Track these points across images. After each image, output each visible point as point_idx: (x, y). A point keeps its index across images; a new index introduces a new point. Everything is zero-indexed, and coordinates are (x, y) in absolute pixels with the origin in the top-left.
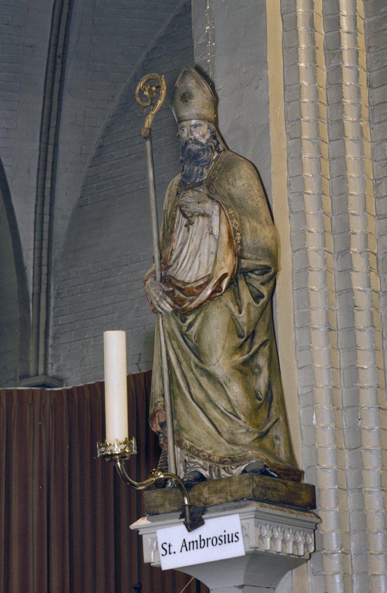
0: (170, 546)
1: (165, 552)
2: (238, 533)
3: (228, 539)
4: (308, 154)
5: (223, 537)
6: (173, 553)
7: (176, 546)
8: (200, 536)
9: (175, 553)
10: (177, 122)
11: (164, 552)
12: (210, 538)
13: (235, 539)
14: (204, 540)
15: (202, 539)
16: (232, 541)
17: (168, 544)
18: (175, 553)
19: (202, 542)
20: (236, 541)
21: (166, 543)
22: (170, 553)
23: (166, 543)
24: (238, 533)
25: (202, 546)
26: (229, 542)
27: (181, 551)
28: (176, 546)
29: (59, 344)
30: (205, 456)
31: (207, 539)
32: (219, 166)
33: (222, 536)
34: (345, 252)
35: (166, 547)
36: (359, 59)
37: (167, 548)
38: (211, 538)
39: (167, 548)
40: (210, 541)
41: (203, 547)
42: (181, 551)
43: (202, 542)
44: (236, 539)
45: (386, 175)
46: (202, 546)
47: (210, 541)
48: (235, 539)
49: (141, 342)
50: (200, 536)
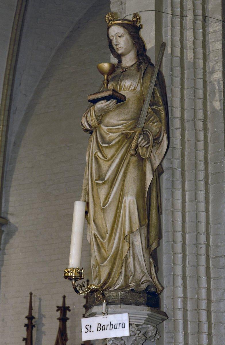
0: (90, 327)
1: (87, 330)
4: (125, 124)
6: (92, 331)
7: (94, 328)
8: (110, 322)
9: (93, 331)
12: (121, 323)
14: (112, 325)
15: (111, 324)
17: (89, 326)
18: (93, 331)
19: (111, 326)
21: (88, 325)
22: (90, 332)
23: (88, 325)
31: (107, 325)
32: (103, 192)
36: (195, 175)
38: (122, 324)
40: (121, 325)
41: (112, 329)
45: (224, 160)
46: (116, 325)
47: (121, 325)
49: (176, 287)
50: (110, 322)
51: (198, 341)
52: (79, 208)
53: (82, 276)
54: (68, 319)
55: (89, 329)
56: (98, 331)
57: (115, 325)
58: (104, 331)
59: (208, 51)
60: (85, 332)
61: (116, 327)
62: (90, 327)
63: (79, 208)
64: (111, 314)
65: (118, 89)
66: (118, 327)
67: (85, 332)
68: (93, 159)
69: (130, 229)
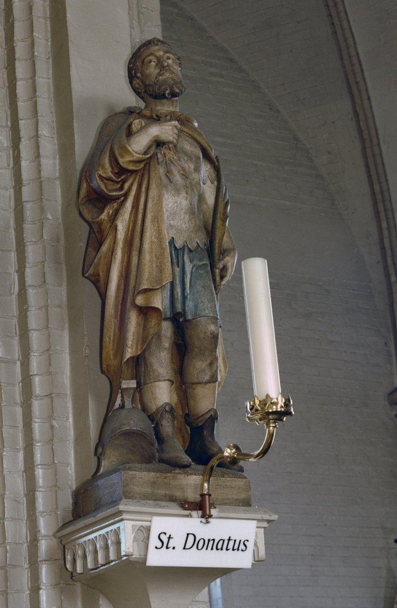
0: (169, 538)
2: (248, 541)
3: (240, 546)
5: (240, 549)
6: (172, 548)
7: (178, 542)
9: (174, 548)
11: (159, 544)
13: (242, 547)
16: (238, 550)
17: (168, 536)
18: (174, 548)
20: (242, 550)
21: (165, 534)
22: (167, 548)
23: (165, 534)
24: (248, 541)
26: (227, 549)
28: (178, 542)
33: (242, 550)
35: (164, 538)
44: (244, 548)
48: (242, 547)
51: (210, 606)
54: (213, 419)
55: (165, 543)
56: (184, 548)
57: (202, 548)
58: (220, 550)
59: (95, 514)
60: (156, 548)
61: (219, 547)
62: (169, 538)
65: (143, 122)
66: (225, 547)
67: (156, 548)
68: (125, 240)
69: (186, 361)
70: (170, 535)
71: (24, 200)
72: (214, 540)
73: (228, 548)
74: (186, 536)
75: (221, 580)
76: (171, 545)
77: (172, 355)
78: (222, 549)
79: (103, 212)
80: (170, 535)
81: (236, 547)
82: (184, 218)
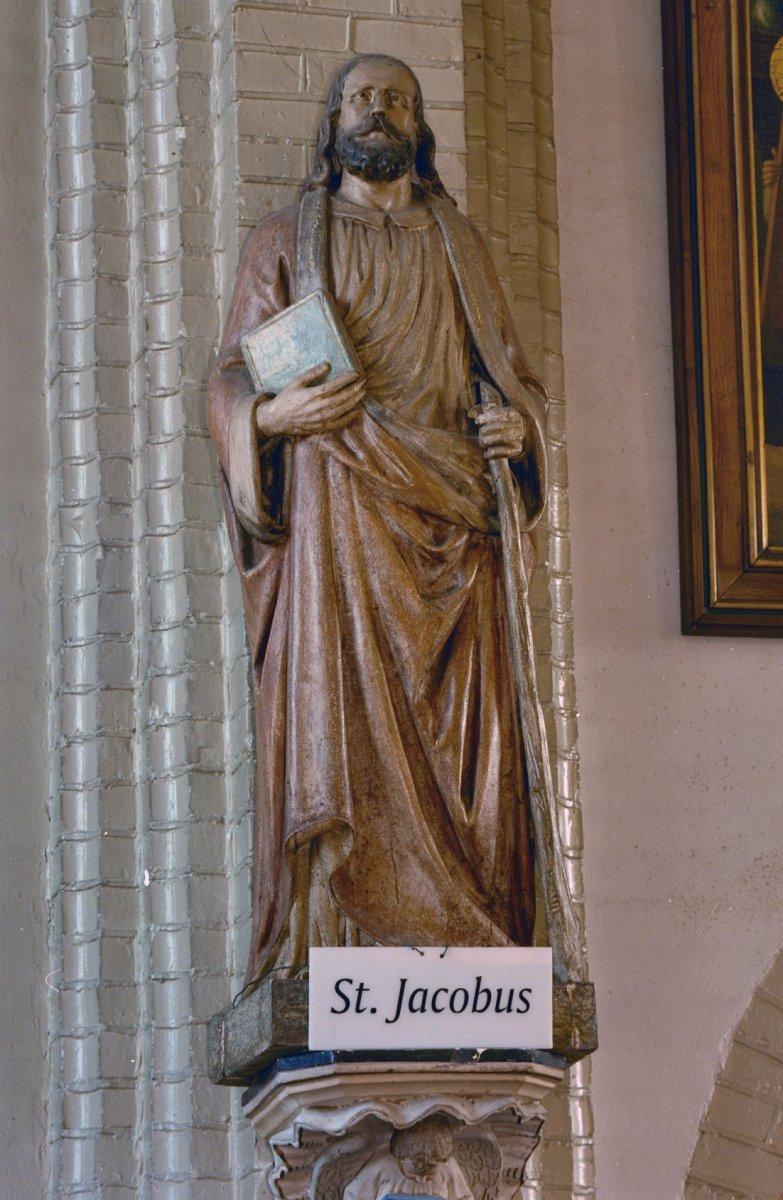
0: (361, 989)
2: (530, 991)
5: (514, 1007)
6: (368, 1011)
7: (382, 997)
8: (479, 979)
10: (529, 529)
13: (517, 1003)
14: (488, 991)
15: (482, 988)
16: (509, 1010)
17: (356, 985)
18: (374, 1011)
19: (483, 998)
20: (519, 1011)
21: (350, 981)
22: (358, 1010)
23: (350, 981)
24: (530, 991)
25: (481, 1004)
27: (403, 982)
29: (269, 181)
30: (507, 1154)
33: (519, 1011)
34: (560, 840)
35: (350, 991)
37: (353, 996)
39: (353, 996)
42: (403, 982)
43: (483, 998)
44: (523, 1007)
46: (480, 1006)
48: (517, 1003)
50: (479, 979)
52: (761, 534)
53: (551, 909)
60: (333, 1011)
61: (417, 1004)
63: (761, 534)
64: (700, 1145)
67: (333, 1011)
70: (362, 985)
71: (459, 112)
72: (498, 1010)
73: (361, 1008)
74: (399, 984)
75: (583, 1065)
76: (367, 1002)
77: (238, 551)
78: (423, 1010)
79: (240, 114)
80: (362, 985)
81: (504, 1004)
82: (263, 114)
